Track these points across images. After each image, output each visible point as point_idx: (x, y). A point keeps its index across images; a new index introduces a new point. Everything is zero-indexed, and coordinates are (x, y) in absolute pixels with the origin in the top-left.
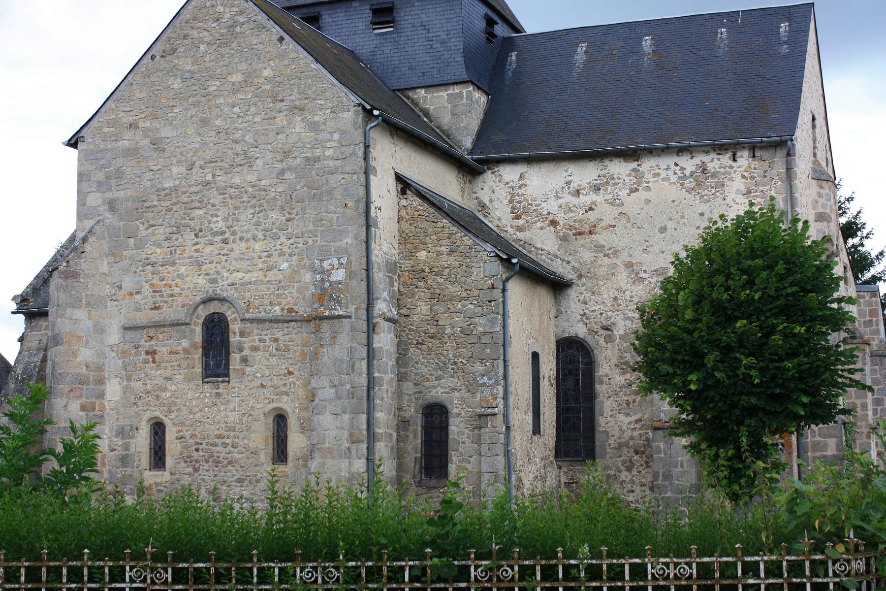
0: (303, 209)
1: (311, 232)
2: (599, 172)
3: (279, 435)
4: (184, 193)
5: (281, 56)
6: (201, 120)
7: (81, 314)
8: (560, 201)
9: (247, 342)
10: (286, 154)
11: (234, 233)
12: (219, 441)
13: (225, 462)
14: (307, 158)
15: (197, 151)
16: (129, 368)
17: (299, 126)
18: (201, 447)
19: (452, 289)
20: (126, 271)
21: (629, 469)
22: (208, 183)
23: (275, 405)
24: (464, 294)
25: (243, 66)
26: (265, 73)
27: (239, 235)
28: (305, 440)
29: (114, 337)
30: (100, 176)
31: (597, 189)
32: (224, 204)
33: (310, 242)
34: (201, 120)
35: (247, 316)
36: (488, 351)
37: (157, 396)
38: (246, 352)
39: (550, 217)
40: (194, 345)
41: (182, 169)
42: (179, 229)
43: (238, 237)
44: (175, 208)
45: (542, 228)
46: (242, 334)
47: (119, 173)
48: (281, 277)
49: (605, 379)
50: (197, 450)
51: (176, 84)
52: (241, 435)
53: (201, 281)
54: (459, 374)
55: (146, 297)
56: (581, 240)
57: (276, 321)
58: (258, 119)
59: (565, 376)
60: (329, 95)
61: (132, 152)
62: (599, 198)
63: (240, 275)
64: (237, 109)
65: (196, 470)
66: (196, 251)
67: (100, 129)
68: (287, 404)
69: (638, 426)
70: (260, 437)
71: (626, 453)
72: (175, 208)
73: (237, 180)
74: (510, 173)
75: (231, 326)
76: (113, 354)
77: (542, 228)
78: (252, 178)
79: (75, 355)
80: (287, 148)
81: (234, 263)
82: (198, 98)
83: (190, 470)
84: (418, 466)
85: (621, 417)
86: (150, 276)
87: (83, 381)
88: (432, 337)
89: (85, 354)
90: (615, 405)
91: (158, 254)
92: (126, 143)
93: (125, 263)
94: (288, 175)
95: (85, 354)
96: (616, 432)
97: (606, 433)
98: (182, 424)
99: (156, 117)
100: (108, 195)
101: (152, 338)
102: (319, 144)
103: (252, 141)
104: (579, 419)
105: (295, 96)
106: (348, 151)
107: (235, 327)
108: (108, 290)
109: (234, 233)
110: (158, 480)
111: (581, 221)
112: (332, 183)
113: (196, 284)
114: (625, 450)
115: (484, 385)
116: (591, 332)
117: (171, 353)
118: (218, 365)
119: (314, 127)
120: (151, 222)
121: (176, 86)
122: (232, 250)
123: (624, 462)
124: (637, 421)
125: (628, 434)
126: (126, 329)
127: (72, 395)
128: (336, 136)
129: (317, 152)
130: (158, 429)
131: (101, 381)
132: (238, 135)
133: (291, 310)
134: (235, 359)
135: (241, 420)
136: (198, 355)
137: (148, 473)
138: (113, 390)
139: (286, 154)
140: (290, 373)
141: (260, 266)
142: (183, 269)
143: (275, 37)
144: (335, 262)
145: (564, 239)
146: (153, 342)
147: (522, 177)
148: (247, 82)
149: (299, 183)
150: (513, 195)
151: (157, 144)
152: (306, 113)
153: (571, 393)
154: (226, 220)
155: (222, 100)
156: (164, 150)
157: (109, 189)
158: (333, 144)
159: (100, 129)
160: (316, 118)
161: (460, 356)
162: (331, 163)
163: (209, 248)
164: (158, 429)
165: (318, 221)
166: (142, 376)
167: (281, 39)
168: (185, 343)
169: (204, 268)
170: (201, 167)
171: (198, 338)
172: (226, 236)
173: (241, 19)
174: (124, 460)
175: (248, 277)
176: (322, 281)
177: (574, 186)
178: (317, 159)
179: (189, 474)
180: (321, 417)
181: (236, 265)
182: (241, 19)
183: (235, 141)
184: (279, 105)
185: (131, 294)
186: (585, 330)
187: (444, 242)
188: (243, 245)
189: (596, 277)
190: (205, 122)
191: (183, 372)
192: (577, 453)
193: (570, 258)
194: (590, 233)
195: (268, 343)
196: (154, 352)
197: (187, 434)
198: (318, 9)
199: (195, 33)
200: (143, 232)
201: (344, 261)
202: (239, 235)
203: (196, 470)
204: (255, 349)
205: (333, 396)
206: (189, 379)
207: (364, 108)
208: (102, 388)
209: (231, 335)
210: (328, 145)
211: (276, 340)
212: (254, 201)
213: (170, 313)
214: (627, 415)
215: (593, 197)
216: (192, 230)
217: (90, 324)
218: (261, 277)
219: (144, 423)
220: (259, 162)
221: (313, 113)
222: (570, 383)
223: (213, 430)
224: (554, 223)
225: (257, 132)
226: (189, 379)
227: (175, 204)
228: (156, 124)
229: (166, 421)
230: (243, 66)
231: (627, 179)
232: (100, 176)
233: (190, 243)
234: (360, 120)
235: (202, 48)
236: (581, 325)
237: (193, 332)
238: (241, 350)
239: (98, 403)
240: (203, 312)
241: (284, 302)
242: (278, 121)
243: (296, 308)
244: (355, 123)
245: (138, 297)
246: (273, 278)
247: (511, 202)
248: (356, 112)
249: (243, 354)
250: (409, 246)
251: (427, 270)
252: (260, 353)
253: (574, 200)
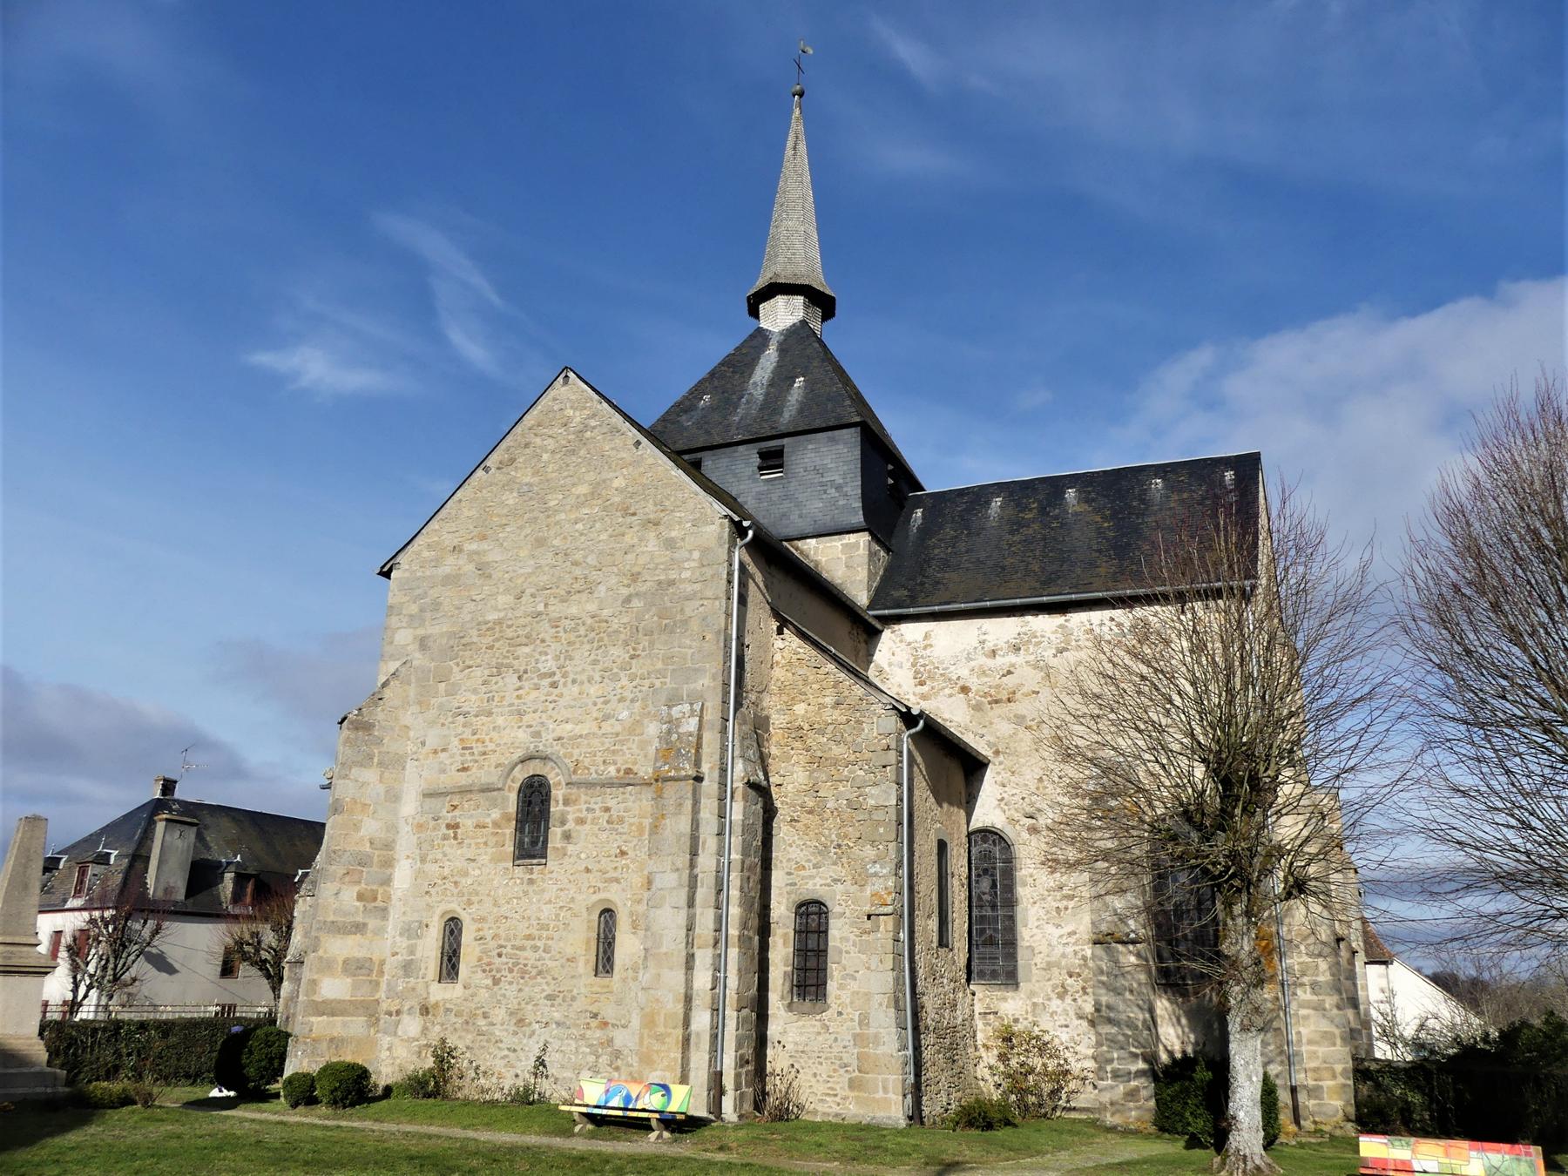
0: (652, 643)
1: (659, 671)
2: (1019, 629)
3: (606, 937)
4: (509, 627)
5: (636, 463)
6: (537, 540)
7: (370, 775)
8: (973, 663)
9: (572, 813)
10: (635, 577)
11: (565, 675)
12: (529, 943)
13: (534, 972)
14: (660, 583)
15: (530, 575)
16: (425, 846)
17: (652, 545)
18: (504, 951)
19: (837, 750)
20: (432, 724)
21: (1061, 996)
22: (540, 614)
23: (602, 895)
24: (852, 758)
25: (591, 476)
26: (616, 483)
27: (571, 676)
28: (637, 942)
29: (409, 806)
30: (414, 609)
31: (1017, 649)
32: (556, 638)
33: (658, 683)
34: (537, 540)
35: (574, 778)
36: (882, 830)
37: (456, 883)
38: (570, 825)
39: (961, 683)
40: (506, 817)
41: (510, 599)
42: (499, 669)
43: (569, 680)
44: (497, 645)
45: (951, 696)
46: (566, 802)
47: (436, 605)
48: (618, 728)
49: (1030, 880)
50: (500, 955)
51: (511, 499)
52: (556, 936)
53: (522, 736)
54: (844, 860)
55: (453, 759)
56: (999, 710)
57: (609, 784)
58: (604, 537)
59: (978, 875)
60: (690, 504)
61: (451, 580)
62: (1018, 660)
63: (569, 727)
64: (579, 526)
65: (496, 982)
66: (519, 697)
67: (418, 553)
68: (617, 897)
69: (1072, 940)
70: (579, 941)
71: (1058, 976)
72: (497, 645)
73: (574, 610)
74: (912, 631)
75: (553, 792)
76: (409, 828)
77: (951, 696)
78: (592, 607)
79: (357, 827)
80: (636, 569)
81: (563, 711)
82: (536, 514)
83: (489, 982)
84: (788, 984)
85: (1050, 929)
86: (460, 729)
87: (363, 861)
88: (810, 812)
89: (370, 827)
90: (1042, 912)
91: (472, 702)
92: (447, 570)
93: (432, 713)
94: (637, 603)
95: (370, 827)
96: (1044, 949)
97: (1031, 948)
98: (483, 919)
99: (484, 538)
100: (421, 632)
101: (455, 807)
102: (674, 563)
103: (594, 563)
104: (996, 930)
105: (651, 507)
106: (709, 572)
107: (558, 793)
108: (410, 748)
109: (565, 675)
110: (448, 996)
111: (998, 686)
112: (688, 612)
113: (519, 739)
114: (1055, 971)
115: (875, 874)
116: (1013, 821)
117: (477, 826)
118: (534, 843)
119: (670, 544)
120: (468, 663)
121: (511, 502)
122: (561, 695)
123: (1055, 987)
124: (1070, 934)
125: (1059, 950)
126: (428, 795)
127: (347, 879)
128: (696, 555)
129: (673, 575)
130: (453, 928)
131: (388, 863)
132: (578, 556)
133: (628, 771)
134: (555, 833)
135: (557, 915)
136: (509, 830)
137: (435, 987)
138: (402, 876)
139: (635, 577)
140: (623, 853)
141: (595, 715)
142: (500, 721)
143: (631, 442)
144: (687, 707)
145: (978, 708)
146: (457, 813)
147: (927, 636)
148: (593, 495)
149: (648, 611)
150: (916, 658)
151: (483, 570)
152: (661, 528)
153: (987, 897)
154: (557, 658)
155: (563, 516)
156: (490, 576)
157: (422, 624)
158: (693, 564)
159: (418, 553)
160: (673, 534)
161: (846, 836)
162: (689, 588)
163: (534, 694)
164: (453, 928)
165: (668, 659)
166: (440, 856)
167: (638, 443)
168: (496, 814)
169: (525, 718)
170: (533, 596)
171: (512, 808)
172: (556, 678)
173: (593, 423)
174: (408, 968)
175: (579, 729)
176: (669, 732)
177: (989, 645)
178: (672, 583)
179: (487, 987)
180: (658, 912)
181: (566, 714)
182: (593, 423)
183: (575, 564)
184: (629, 519)
185: (435, 752)
186: (1003, 818)
187: (827, 692)
188: (576, 689)
189: (1015, 753)
190: (541, 542)
191: (490, 850)
192: (994, 975)
193: (984, 731)
194: (1009, 700)
195: (598, 813)
196: (456, 826)
197: (489, 934)
198: (699, 455)
199: (538, 440)
200: (457, 676)
201: (697, 707)
202: (571, 676)
203: (496, 982)
204: (581, 821)
205: (674, 884)
206: (496, 860)
207: (731, 520)
208: (388, 871)
209: (552, 803)
210: (686, 565)
211: (607, 810)
212: (593, 634)
213: (484, 774)
214: (1058, 926)
215: (1012, 658)
216: (515, 671)
217: (381, 789)
218: (595, 729)
219: (436, 918)
220: (602, 588)
221: (670, 527)
222: (985, 884)
223: (522, 928)
224: (965, 690)
225: (601, 553)
226: (496, 860)
227: (498, 640)
228: (485, 546)
229: (464, 916)
230: (591, 476)
231: (1053, 637)
232: (414, 609)
233: (512, 687)
234: (726, 535)
235: (545, 457)
236: (998, 811)
237: (505, 799)
238: (563, 823)
239: (381, 891)
240: (520, 775)
241: (620, 760)
242: (627, 538)
243: (635, 769)
244: (720, 538)
245: (442, 755)
246: (609, 730)
247: (914, 665)
248: (722, 525)
249: (566, 828)
250: (785, 698)
251: (806, 727)
252: (587, 827)
253: (990, 663)
